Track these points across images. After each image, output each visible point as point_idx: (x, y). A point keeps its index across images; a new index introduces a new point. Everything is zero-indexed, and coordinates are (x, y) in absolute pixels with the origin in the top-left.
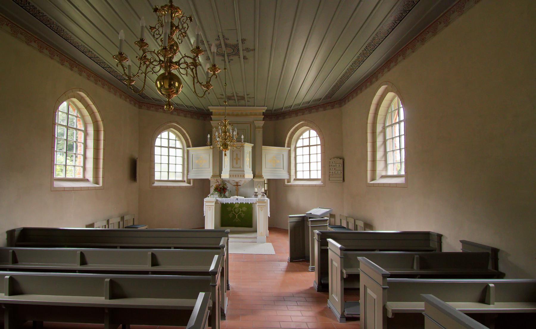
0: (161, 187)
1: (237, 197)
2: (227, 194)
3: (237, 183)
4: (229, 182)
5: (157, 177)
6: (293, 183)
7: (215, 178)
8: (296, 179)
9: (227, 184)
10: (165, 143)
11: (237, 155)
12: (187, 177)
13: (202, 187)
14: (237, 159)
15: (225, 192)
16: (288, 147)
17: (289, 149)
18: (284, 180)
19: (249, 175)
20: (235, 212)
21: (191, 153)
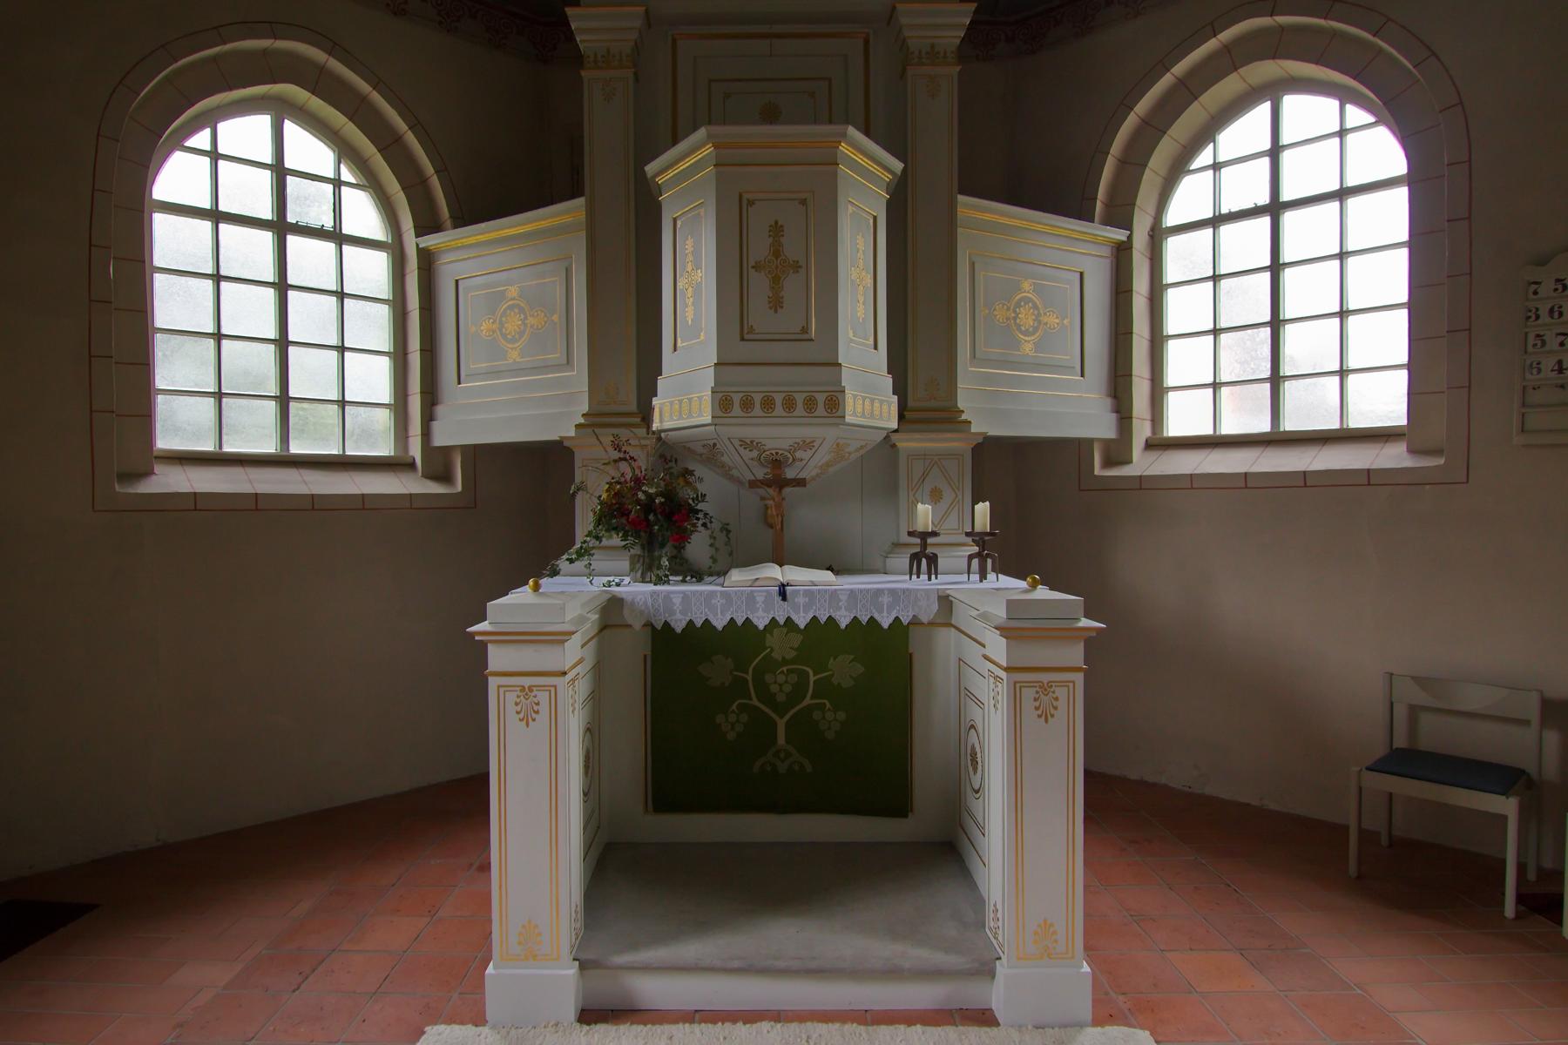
0: (197, 502)
1: (774, 572)
2: (698, 547)
3: (777, 463)
4: (711, 453)
5: (180, 423)
6: (1142, 464)
7: (607, 437)
8: (1161, 444)
9: (700, 470)
10: (249, 192)
11: (777, 230)
12: (426, 434)
13: (512, 507)
14: (773, 272)
15: (682, 538)
16: (1109, 221)
17: (1120, 235)
18: (1080, 447)
19: (870, 402)
20: (767, 697)
21: (449, 270)
